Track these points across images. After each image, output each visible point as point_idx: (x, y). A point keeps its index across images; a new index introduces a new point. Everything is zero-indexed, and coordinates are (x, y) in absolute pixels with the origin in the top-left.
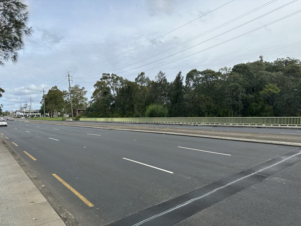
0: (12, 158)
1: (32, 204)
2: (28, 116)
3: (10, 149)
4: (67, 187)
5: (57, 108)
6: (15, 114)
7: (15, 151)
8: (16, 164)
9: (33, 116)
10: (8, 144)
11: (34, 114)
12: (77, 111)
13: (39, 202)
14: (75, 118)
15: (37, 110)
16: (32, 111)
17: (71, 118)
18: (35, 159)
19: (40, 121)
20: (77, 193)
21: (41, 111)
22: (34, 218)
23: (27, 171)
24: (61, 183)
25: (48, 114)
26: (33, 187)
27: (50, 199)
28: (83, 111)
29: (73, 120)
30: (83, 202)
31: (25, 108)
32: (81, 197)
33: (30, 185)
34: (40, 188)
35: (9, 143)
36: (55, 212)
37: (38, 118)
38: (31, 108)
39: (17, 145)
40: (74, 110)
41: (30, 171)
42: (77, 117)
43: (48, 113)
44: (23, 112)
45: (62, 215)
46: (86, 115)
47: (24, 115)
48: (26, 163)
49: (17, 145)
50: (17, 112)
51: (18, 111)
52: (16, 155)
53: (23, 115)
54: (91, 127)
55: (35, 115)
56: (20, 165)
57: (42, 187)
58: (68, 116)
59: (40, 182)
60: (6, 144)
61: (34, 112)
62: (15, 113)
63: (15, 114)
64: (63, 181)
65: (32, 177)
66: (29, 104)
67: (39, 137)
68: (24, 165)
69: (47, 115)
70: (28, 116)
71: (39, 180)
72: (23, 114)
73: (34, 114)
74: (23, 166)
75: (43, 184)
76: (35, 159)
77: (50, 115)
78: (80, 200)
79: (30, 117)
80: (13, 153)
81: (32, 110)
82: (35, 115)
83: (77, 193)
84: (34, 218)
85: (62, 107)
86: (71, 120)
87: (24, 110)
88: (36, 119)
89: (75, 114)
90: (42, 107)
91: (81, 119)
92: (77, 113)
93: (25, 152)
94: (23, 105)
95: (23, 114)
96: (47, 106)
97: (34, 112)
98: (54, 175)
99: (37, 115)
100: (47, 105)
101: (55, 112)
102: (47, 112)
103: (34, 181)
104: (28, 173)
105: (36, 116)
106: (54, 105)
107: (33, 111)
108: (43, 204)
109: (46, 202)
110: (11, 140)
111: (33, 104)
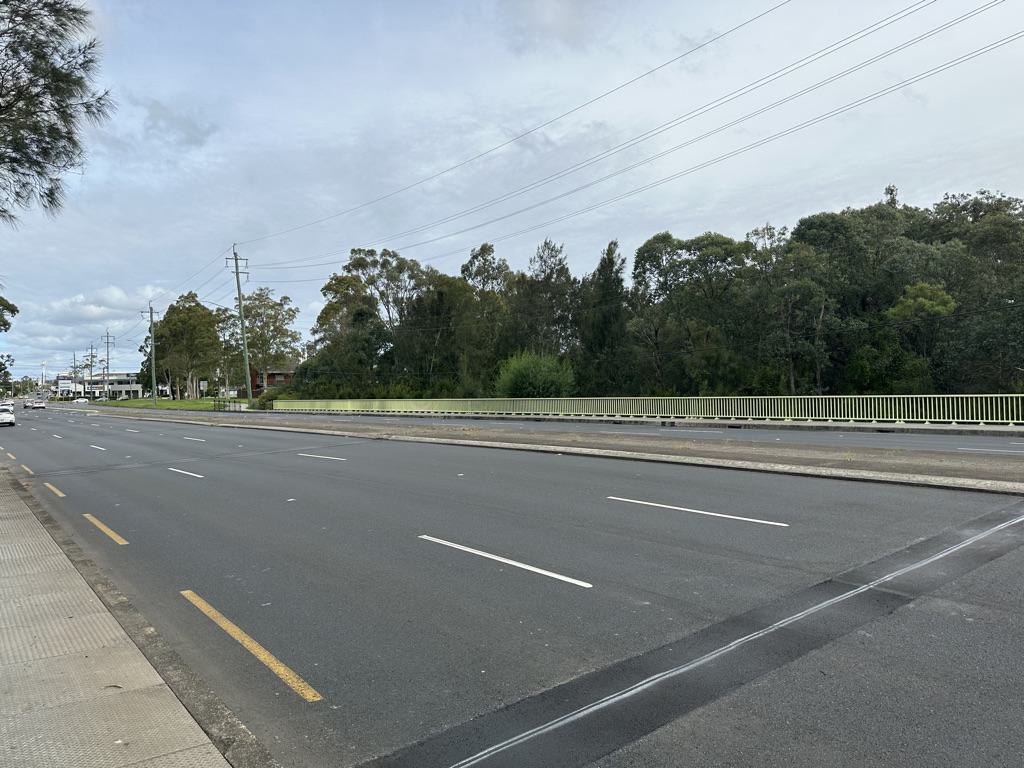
0: (44, 536)
1: (111, 692)
2: (97, 394)
3: (38, 505)
4: (233, 634)
5: (196, 367)
6: (53, 388)
7: (55, 515)
8: (60, 558)
9: (114, 396)
10: (32, 491)
11: (117, 387)
12: (265, 376)
13: (137, 687)
14: (257, 400)
15: (128, 375)
16: (110, 378)
17: (246, 400)
18: (122, 542)
19: (137, 411)
20: (264, 656)
21: (144, 379)
22: (120, 742)
23: (96, 583)
24: (210, 622)
25: (167, 389)
26: (118, 634)
27: (175, 675)
28: (286, 376)
29: (252, 407)
30: (285, 684)
31: (87, 366)
32: (281, 670)
33: (108, 628)
34: (141, 639)
35: (35, 486)
36: (191, 720)
37: (133, 402)
38: (107, 368)
39: (61, 495)
40: (255, 375)
41: (107, 579)
42: (263, 398)
43: (164, 384)
44: (80, 383)
45: (214, 730)
46: (296, 389)
47: (85, 393)
48: (92, 554)
49: (61, 495)
50: (60, 382)
51: (64, 378)
52: (57, 528)
53: (80, 393)
54: (314, 431)
55: (124, 392)
56: (72, 561)
57: (148, 636)
58: (233, 394)
59: (140, 617)
60: (25, 490)
61: (120, 382)
62: (56, 383)
63: (53, 388)
64: (219, 614)
65: (113, 602)
66: (101, 354)
67: (137, 465)
68: (84, 562)
69: (162, 391)
70: (97, 394)
71: (136, 610)
72: (80, 388)
73: (117, 387)
74: (81, 564)
75: (151, 625)
76: (122, 542)
77: (173, 392)
78: (277, 678)
79: (104, 399)
80: (47, 521)
81: (112, 375)
82: (124, 392)
83: (264, 656)
84: (120, 742)
85: (215, 364)
86: (244, 407)
87: (86, 375)
88: (125, 403)
89: (257, 388)
90: (147, 365)
91: (279, 405)
92: (265, 384)
93: (87, 516)
94: (81, 357)
95: (80, 388)
96: (161, 362)
97: (120, 382)
98: (187, 594)
99: (128, 392)
100: (163, 358)
101: (189, 382)
102: (161, 381)
103: (119, 613)
104: (99, 588)
105: (124, 396)
106: (185, 358)
107: (114, 378)
108: (149, 692)
109: (160, 685)
110: (40, 476)
111: (114, 353)
